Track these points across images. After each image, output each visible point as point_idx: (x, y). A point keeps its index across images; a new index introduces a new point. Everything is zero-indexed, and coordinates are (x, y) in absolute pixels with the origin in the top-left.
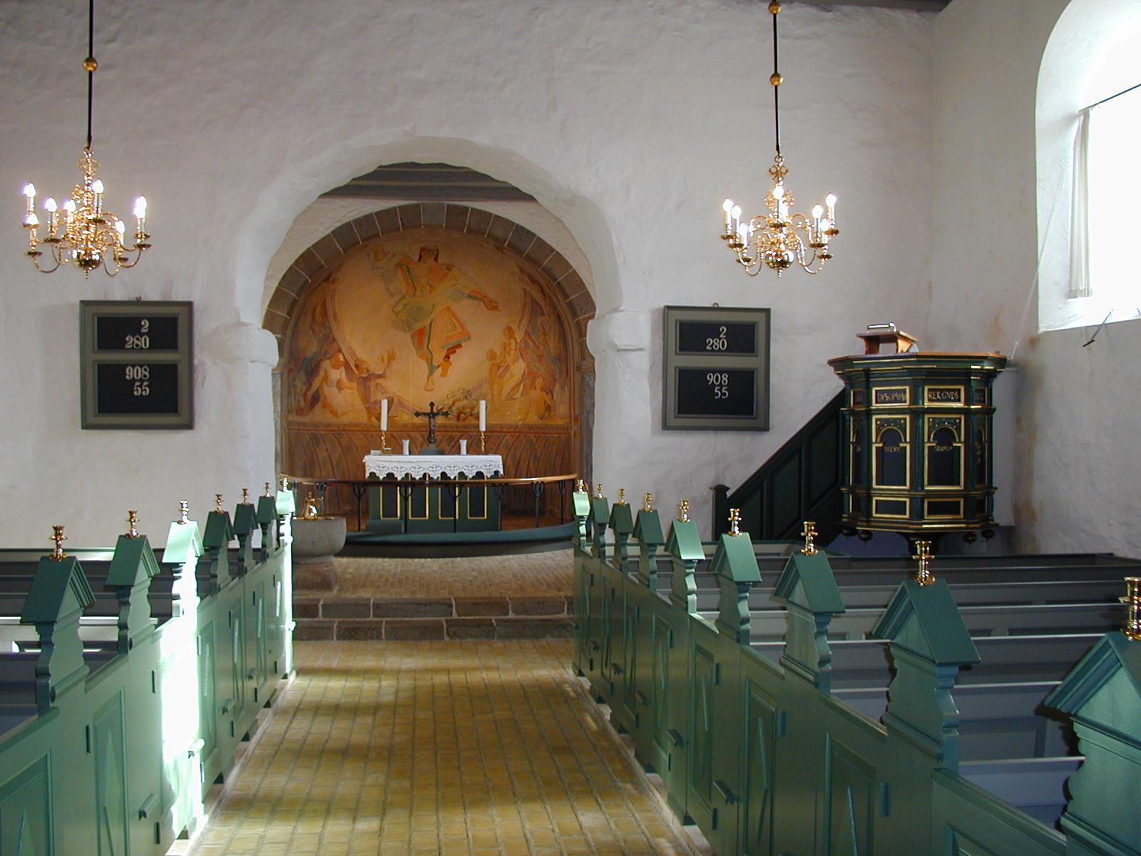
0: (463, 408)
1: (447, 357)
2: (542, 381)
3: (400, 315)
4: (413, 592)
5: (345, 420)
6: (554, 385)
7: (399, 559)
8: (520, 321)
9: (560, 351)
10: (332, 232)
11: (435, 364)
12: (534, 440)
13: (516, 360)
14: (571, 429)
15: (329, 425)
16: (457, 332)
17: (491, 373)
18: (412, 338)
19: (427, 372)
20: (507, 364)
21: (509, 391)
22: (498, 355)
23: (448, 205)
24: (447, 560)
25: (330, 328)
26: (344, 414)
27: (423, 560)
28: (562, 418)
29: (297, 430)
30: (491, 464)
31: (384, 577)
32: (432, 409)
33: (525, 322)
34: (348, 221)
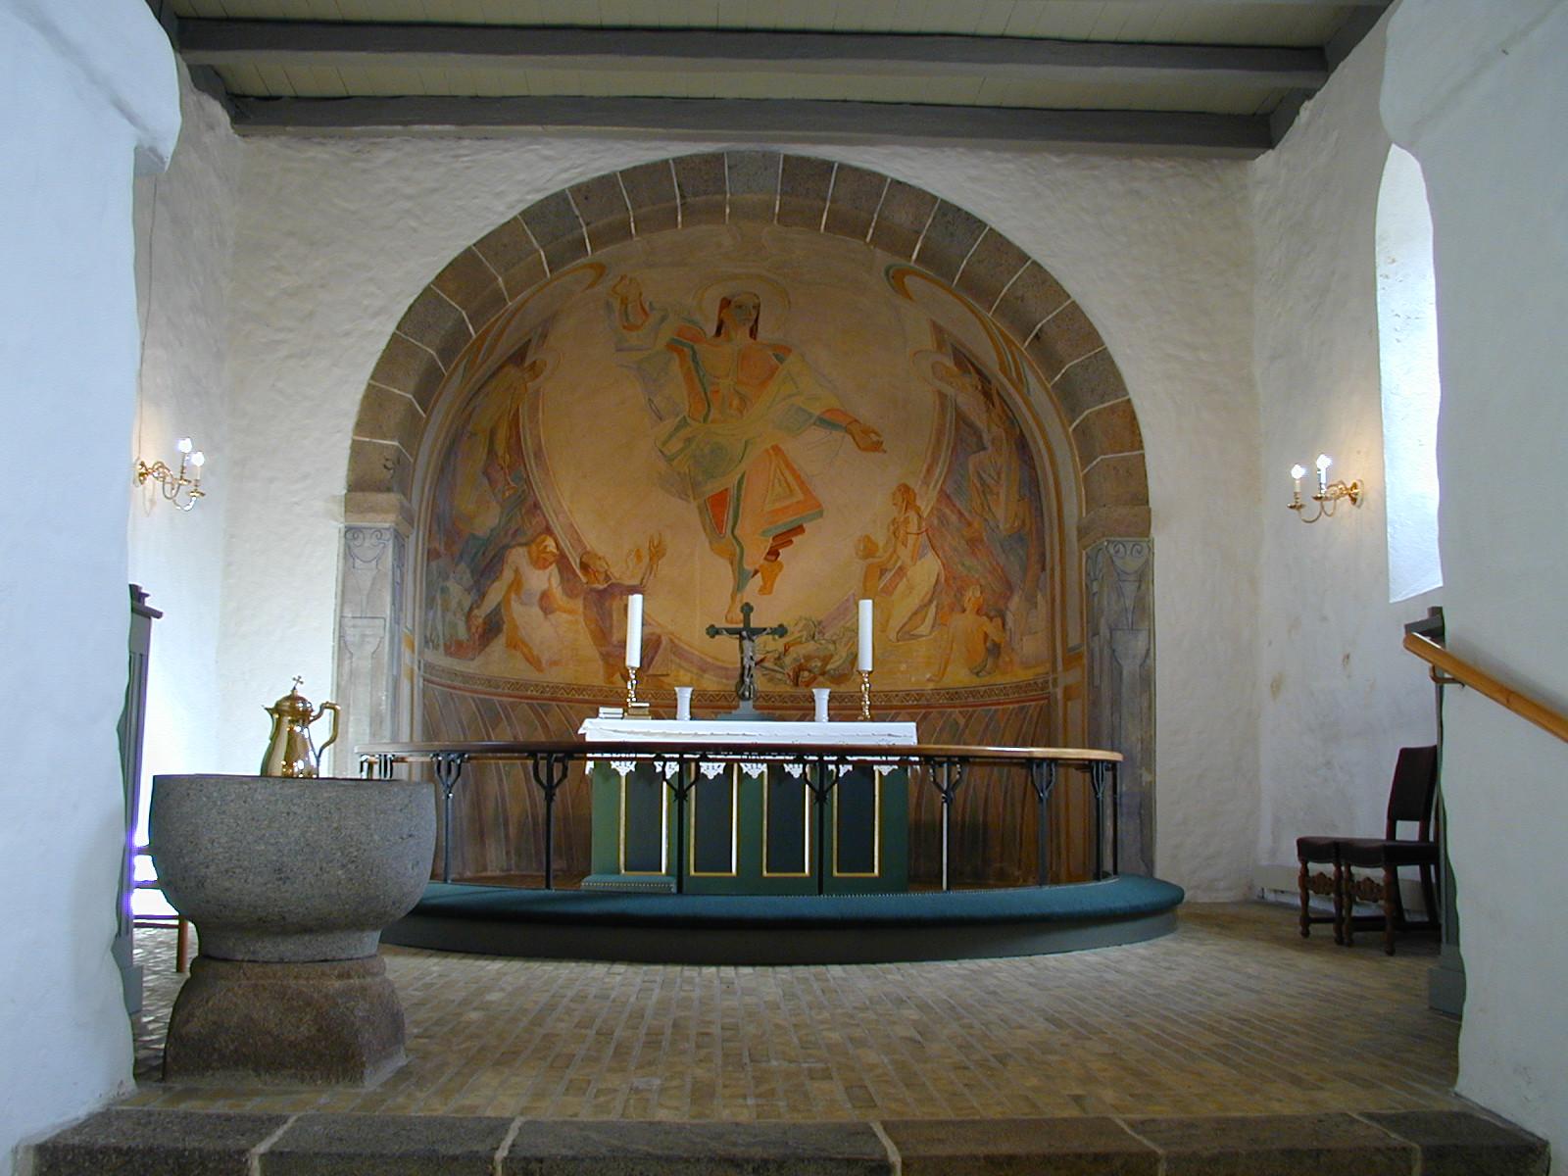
0: (808, 658)
1: (774, 553)
2: (978, 594)
3: (675, 463)
4: (702, 1093)
5: (555, 676)
6: (1008, 599)
7: (659, 968)
8: (928, 471)
9: (1024, 521)
10: (523, 213)
11: (748, 567)
12: (962, 721)
13: (917, 556)
14: (1055, 684)
15: (517, 685)
16: (795, 500)
17: (865, 586)
18: (700, 513)
19: (730, 585)
20: (899, 564)
21: (906, 619)
22: (881, 545)
23: (787, 158)
24: (801, 971)
25: (528, 482)
26: (554, 663)
27: (728, 971)
28: (1026, 666)
29: (449, 687)
30: (904, 733)
31: (598, 1022)
32: (747, 620)
33: (939, 470)
34: (557, 189)
